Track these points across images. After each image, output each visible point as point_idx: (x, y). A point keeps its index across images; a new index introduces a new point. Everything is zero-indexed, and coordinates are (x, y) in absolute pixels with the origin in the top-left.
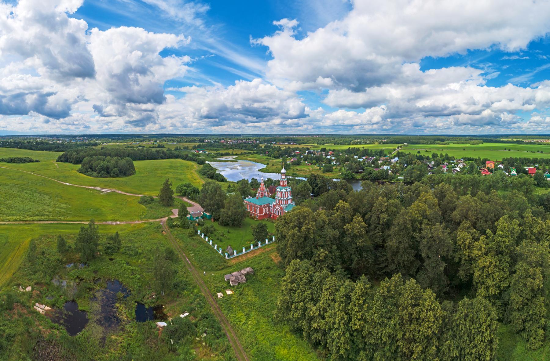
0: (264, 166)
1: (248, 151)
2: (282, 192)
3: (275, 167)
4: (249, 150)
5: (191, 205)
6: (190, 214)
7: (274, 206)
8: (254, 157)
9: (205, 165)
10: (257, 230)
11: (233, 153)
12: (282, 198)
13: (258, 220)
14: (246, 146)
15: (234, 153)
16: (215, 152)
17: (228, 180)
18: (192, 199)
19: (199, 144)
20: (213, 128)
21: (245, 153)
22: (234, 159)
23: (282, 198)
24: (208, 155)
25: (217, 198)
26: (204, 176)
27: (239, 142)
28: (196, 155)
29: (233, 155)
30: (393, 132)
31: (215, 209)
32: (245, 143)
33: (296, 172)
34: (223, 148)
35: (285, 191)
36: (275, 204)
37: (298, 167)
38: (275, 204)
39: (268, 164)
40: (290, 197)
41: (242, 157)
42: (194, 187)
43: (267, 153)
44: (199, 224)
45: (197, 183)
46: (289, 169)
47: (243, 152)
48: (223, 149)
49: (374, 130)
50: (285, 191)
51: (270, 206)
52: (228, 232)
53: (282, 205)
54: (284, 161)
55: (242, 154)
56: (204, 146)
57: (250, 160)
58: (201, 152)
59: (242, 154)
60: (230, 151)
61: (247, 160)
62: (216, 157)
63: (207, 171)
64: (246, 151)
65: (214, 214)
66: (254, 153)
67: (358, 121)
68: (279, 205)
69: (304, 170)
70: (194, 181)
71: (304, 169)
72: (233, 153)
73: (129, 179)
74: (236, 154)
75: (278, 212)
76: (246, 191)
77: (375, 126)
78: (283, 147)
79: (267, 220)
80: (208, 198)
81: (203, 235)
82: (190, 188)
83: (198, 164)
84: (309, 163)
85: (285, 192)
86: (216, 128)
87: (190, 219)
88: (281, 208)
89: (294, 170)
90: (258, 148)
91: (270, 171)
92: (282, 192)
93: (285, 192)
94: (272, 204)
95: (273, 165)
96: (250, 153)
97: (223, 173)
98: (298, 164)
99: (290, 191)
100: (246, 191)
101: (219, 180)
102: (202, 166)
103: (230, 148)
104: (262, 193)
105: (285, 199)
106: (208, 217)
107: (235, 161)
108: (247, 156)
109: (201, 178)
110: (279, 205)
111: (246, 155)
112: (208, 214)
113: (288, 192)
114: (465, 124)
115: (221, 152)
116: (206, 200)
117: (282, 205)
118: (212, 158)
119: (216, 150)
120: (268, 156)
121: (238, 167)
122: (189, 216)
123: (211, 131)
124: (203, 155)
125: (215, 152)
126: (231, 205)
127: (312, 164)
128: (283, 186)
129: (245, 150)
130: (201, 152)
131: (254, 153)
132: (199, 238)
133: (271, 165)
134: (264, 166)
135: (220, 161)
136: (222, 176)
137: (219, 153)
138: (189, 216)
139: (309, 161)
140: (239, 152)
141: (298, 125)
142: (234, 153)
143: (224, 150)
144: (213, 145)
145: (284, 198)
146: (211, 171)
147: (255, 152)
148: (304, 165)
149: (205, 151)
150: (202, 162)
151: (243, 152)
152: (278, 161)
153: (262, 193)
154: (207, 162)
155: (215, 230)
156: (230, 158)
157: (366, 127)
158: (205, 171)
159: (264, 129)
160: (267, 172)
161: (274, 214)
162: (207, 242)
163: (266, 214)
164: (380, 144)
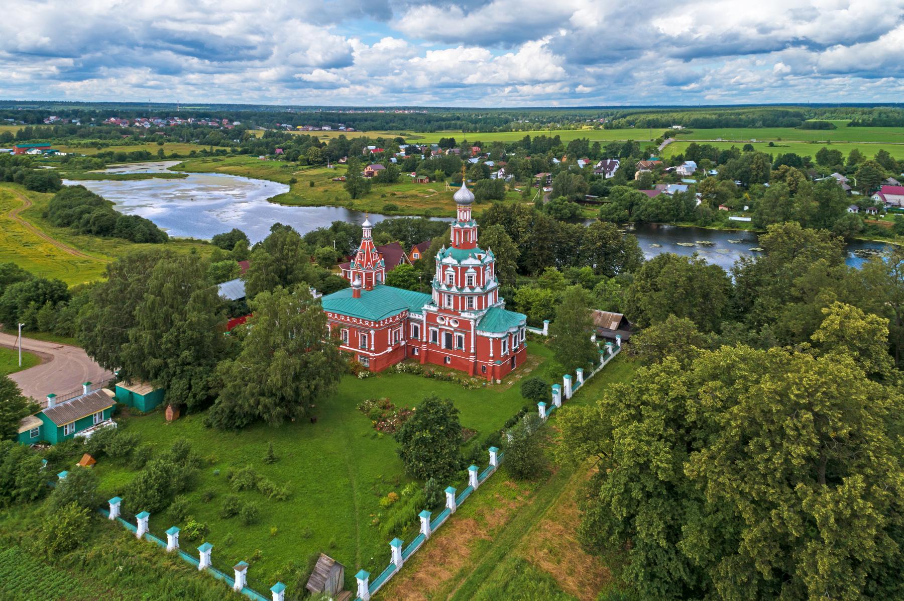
0: (284, 189)
1: (215, 148)
2: (465, 269)
3: (322, 189)
4: (217, 144)
5: (32, 360)
6: (36, 410)
7: (431, 317)
8: (240, 164)
9: (61, 191)
10: (427, 434)
11: (161, 152)
12: (467, 290)
13: (371, 375)
14: (205, 135)
15: (167, 153)
16: (95, 151)
17: (171, 233)
18: (32, 330)
19: (23, 128)
20: (64, 85)
21: (204, 151)
22: (171, 169)
23: (467, 290)
24: (65, 160)
25: (193, 317)
26: (67, 230)
27: (172, 123)
28: (16, 163)
29: (162, 157)
30: (607, 100)
31: (185, 364)
32: (195, 126)
33: (392, 203)
34: (119, 138)
35: (478, 262)
36: (434, 309)
37: (389, 189)
38: (434, 309)
39: (293, 182)
40: (493, 284)
41: (196, 163)
42: (36, 275)
43: (278, 151)
44: (99, 455)
45: (38, 256)
46: (368, 193)
47: (199, 149)
48: (118, 142)
49: (548, 97)
50: (478, 262)
51: (409, 320)
52: (272, 460)
53: (465, 315)
54: (354, 171)
55: (193, 155)
56: (45, 135)
57: (225, 172)
58: (35, 152)
59: (193, 155)
60: (153, 149)
61: (218, 172)
62: (100, 166)
63: (78, 209)
64: (208, 148)
65: (178, 385)
66: (234, 151)
67: (503, 75)
68: (455, 313)
69: (416, 196)
70: (25, 251)
71: (414, 192)
72: (161, 152)
73: (307, 211)
74: (175, 157)
75: (449, 337)
76: (289, 270)
77: (550, 89)
78: (327, 135)
79: (410, 371)
80: (146, 323)
81: (142, 521)
82: (17, 285)
83: (32, 188)
84: (423, 177)
85: (476, 268)
86: (77, 85)
87: (41, 437)
88: (464, 325)
89: (383, 196)
90: (247, 139)
91: (309, 200)
92: (465, 269)
93: (476, 268)
94: (420, 312)
95: (312, 185)
96: (224, 153)
97: (147, 213)
98: (390, 178)
99: (490, 264)
100: (289, 270)
101: (138, 236)
102: (51, 195)
103: (146, 140)
104: (369, 275)
105: (478, 290)
106: (142, 404)
107: (179, 174)
108: (214, 160)
109: (55, 236)
110: (455, 313)
111: (210, 158)
112: (142, 390)
113: (485, 267)
114: (839, 73)
115: (117, 150)
116: (131, 332)
117: (465, 315)
118: (87, 167)
119: (94, 145)
120: (287, 159)
121: (193, 193)
122: (32, 424)
123: (62, 93)
124: (46, 162)
125: (95, 151)
126: (279, 339)
127: (431, 179)
128: (466, 246)
129: (201, 144)
130: (35, 152)
131: (234, 151)
132: (119, 544)
133: (303, 184)
134: (284, 189)
135: (111, 177)
136: (148, 223)
137: (110, 154)
138: (32, 424)
139: (423, 171)
140: (185, 149)
141: (333, 86)
142: (167, 153)
143: (127, 144)
144: (79, 132)
145: (472, 288)
146: (97, 212)
147: (239, 149)
148: (407, 183)
149: (53, 148)
150: (48, 184)
151: (199, 149)
152: (325, 174)
153: (369, 275)
154: (66, 182)
155: (200, 464)
156: (153, 167)
157: (526, 89)
158: (68, 211)
159: (239, 92)
160: (300, 205)
161: (433, 345)
162: (173, 556)
163: (397, 349)
164: (597, 128)
